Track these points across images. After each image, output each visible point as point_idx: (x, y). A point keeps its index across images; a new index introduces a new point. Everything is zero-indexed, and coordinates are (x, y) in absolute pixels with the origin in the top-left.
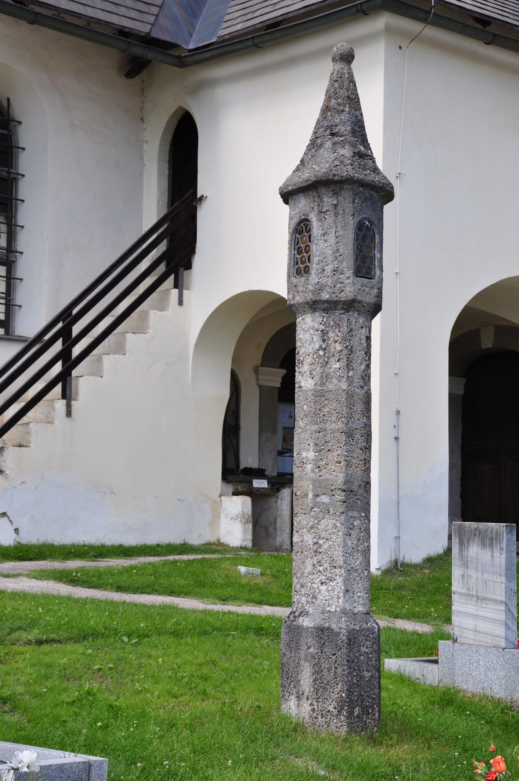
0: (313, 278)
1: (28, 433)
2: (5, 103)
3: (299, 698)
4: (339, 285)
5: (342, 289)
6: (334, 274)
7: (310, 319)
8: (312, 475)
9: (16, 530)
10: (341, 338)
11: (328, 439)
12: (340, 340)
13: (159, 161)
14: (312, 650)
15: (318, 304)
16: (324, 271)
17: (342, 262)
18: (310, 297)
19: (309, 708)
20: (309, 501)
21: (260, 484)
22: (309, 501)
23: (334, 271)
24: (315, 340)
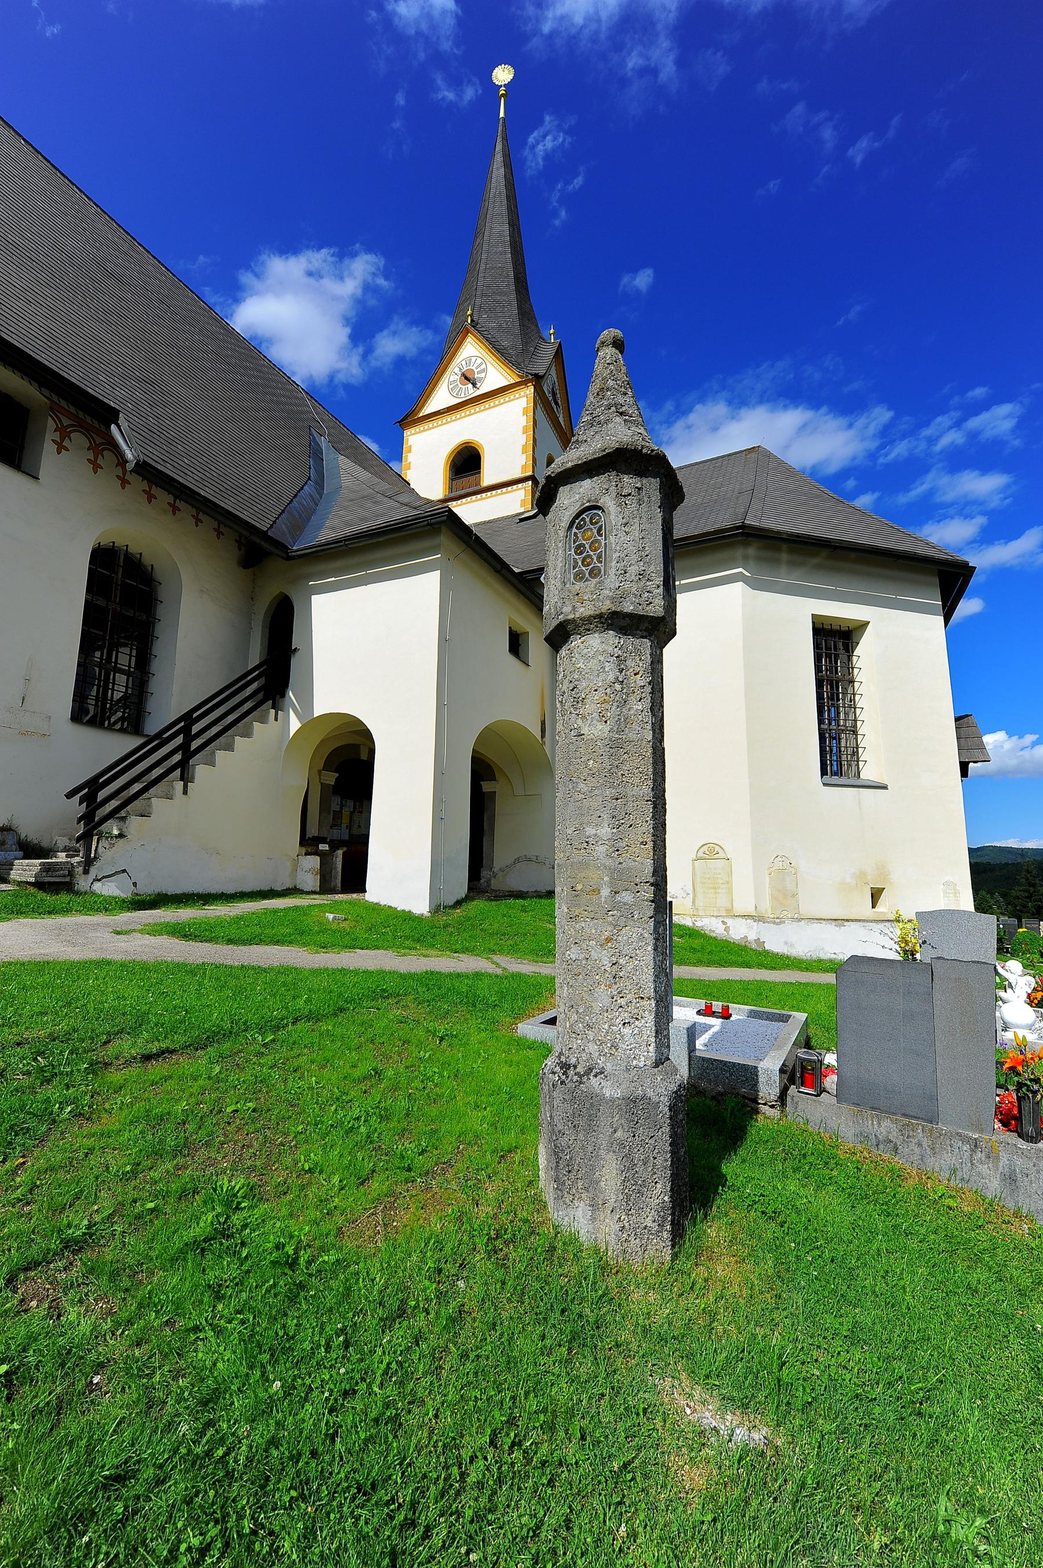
0: (612, 580)
1: (150, 806)
2: (150, 568)
3: (594, 1206)
4: (646, 594)
8: (609, 862)
9: (135, 884)
11: (630, 810)
12: (641, 673)
14: (619, 1134)
17: (649, 564)
18: (606, 606)
19: (617, 1227)
20: (603, 899)
21: (324, 847)
22: (603, 899)
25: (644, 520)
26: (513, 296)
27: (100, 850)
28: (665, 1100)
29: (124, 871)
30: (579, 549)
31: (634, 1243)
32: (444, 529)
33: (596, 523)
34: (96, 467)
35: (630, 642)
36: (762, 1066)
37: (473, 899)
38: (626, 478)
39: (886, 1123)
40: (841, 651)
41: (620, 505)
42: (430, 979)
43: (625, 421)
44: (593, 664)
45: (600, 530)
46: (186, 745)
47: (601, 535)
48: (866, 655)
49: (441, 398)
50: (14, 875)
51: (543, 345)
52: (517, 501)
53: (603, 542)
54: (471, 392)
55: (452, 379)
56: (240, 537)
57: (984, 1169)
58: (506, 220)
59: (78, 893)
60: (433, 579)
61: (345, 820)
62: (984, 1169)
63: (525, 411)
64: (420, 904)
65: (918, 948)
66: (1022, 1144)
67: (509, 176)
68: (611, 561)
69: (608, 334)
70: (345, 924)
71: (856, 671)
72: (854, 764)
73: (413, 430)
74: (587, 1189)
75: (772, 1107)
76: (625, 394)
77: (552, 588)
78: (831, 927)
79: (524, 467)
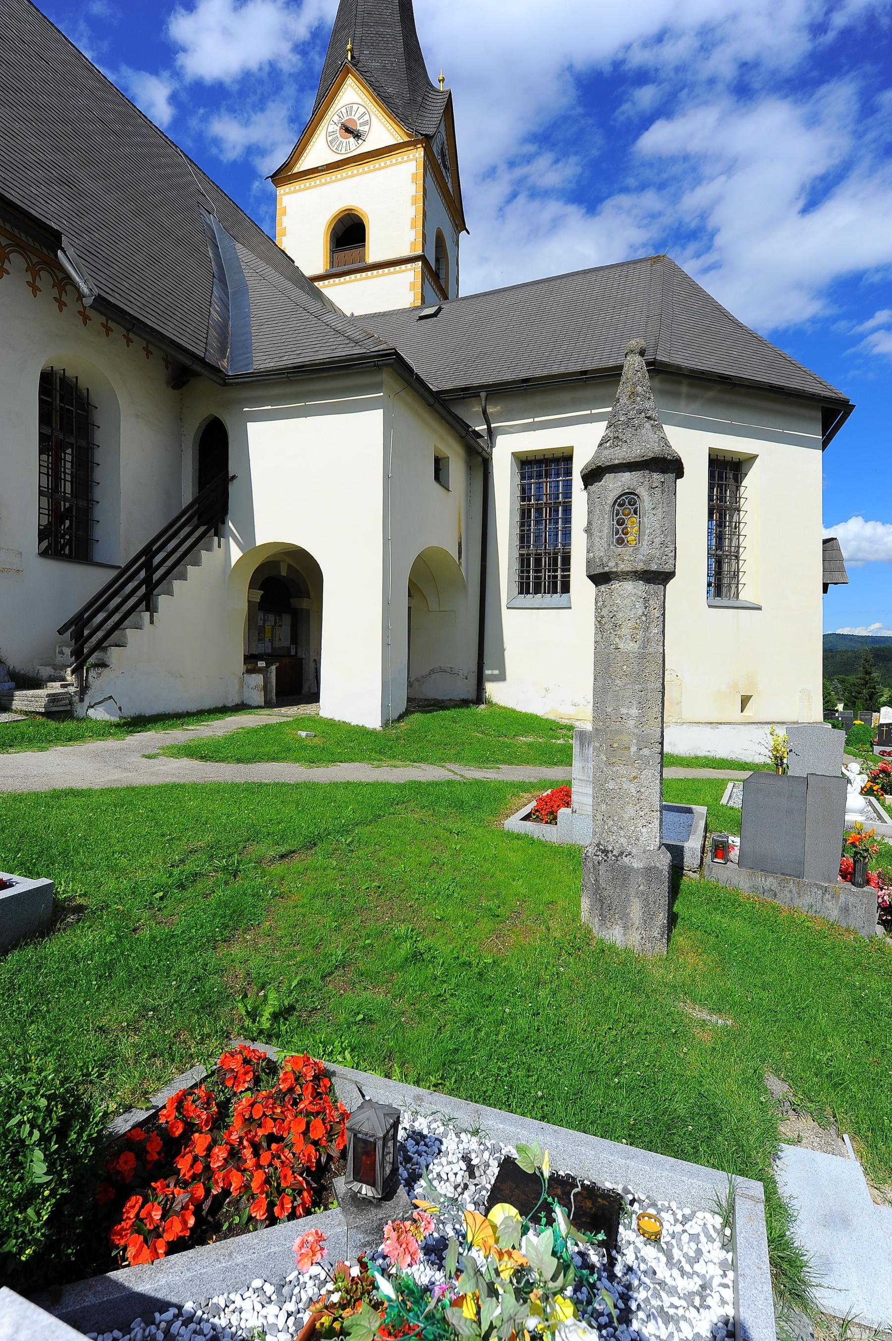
0: (645, 549)
1: (125, 636)
2: (85, 392)
3: (625, 927)
8: (636, 731)
9: (120, 708)
11: (649, 698)
13: (193, 449)
14: (641, 887)
18: (640, 567)
26: (399, 29)
27: (90, 679)
28: (666, 868)
29: (111, 697)
31: (648, 945)
34: (35, 290)
36: (687, 845)
37: (413, 712)
38: (655, 476)
39: (770, 879)
40: (732, 481)
42: (416, 787)
46: (146, 579)
48: (753, 485)
49: (317, 153)
50: (17, 704)
54: (354, 147)
55: (330, 130)
56: (167, 355)
57: (829, 904)
59: (80, 720)
60: (376, 417)
61: (268, 635)
62: (829, 904)
64: (372, 719)
65: (785, 755)
66: (854, 889)
70: (316, 740)
71: (742, 501)
72: (733, 586)
74: (621, 919)
75: (694, 872)
78: (707, 729)
79: (413, 244)
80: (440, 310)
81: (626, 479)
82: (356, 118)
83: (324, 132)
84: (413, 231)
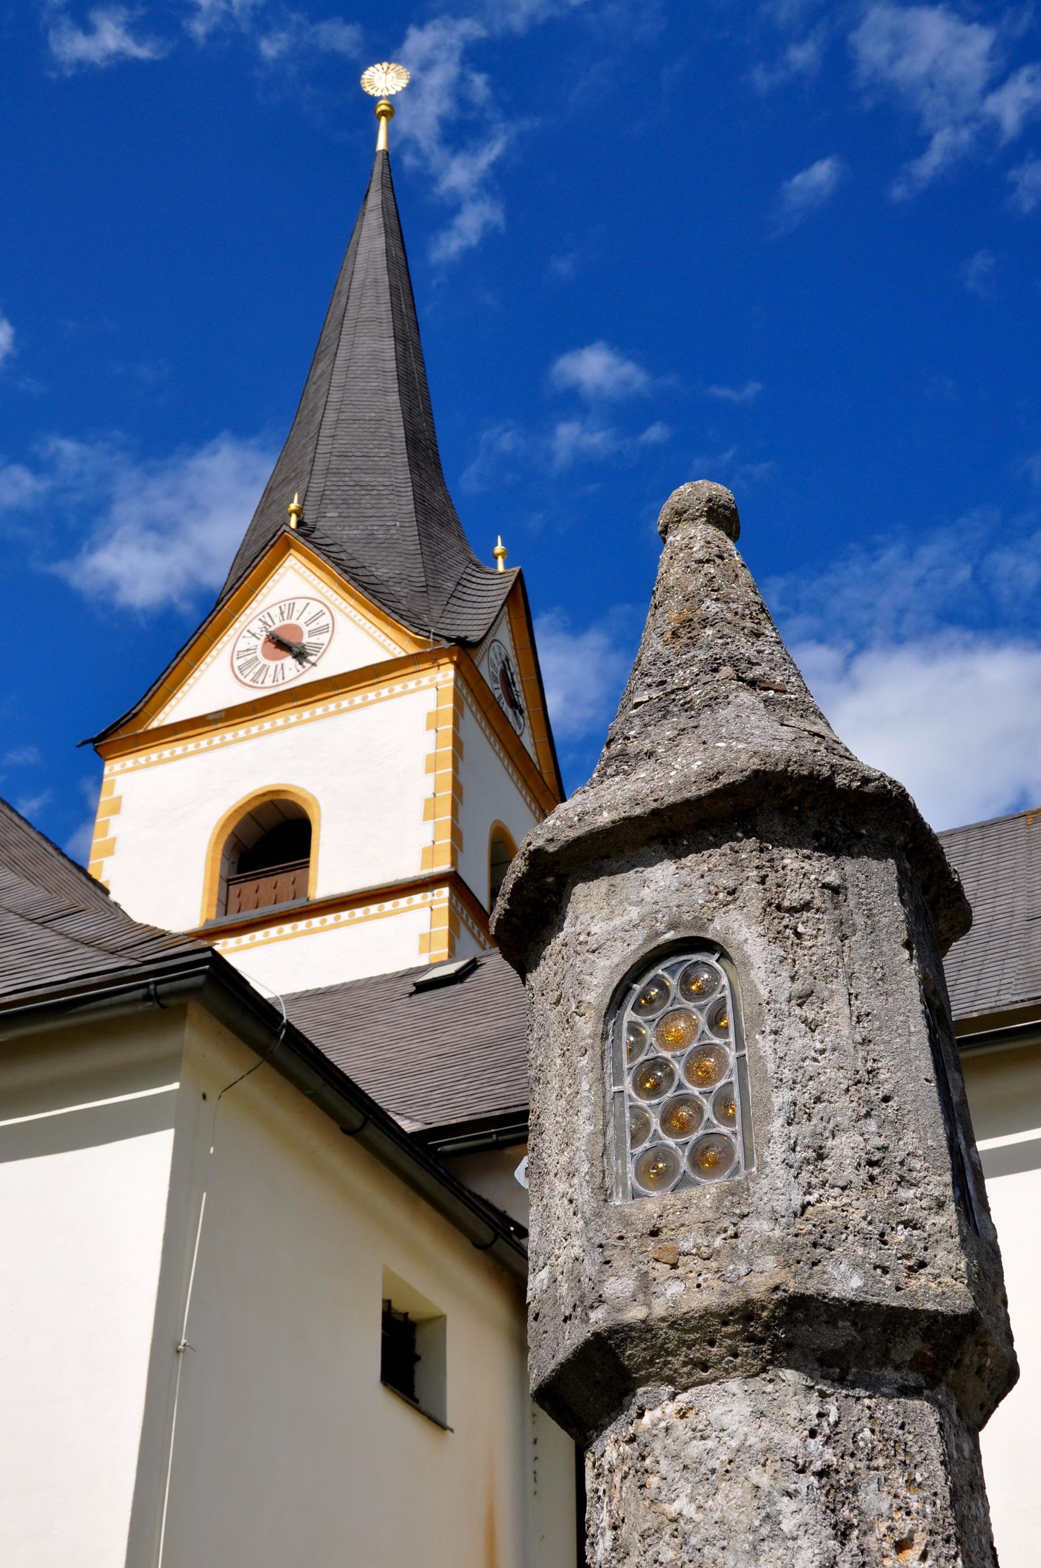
0: (776, 1186)
4: (902, 1234)
5: (919, 1253)
6: (872, 1178)
7: (742, 1408)
10: (926, 1523)
12: (921, 1540)
15: (809, 1320)
16: (821, 1157)
17: (897, 1125)
18: (764, 1277)
23: (871, 1163)
24: (788, 1525)
25: (862, 985)
30: (652, 1076)
32: (195, 1010)
33: (702, 993)
35: (863, 1412)
38: (790, 859)
41: (778, 937)
43: (766, 701)
44: (730, 1501)
45: (715, 1021)
47: (723, 1032)
49: (211, 684)
51: (480, 578)
52: (412, 937)
53: (732, 1055)
54: (291, 673)
55: (242, 645)
58: (388, 329)
60: (145, 1162)
63: (433, 721)
67: (396, 251)
68: (767, 1117)
69: (694, 491)
73: (129, 761)
76: (758, 635)
77: (560, 1207)
79: (430, 853)
80: (472, 967)
81: (660, 890)
82: (301, 623)
83: (228, 649)
84: (429, 826)
